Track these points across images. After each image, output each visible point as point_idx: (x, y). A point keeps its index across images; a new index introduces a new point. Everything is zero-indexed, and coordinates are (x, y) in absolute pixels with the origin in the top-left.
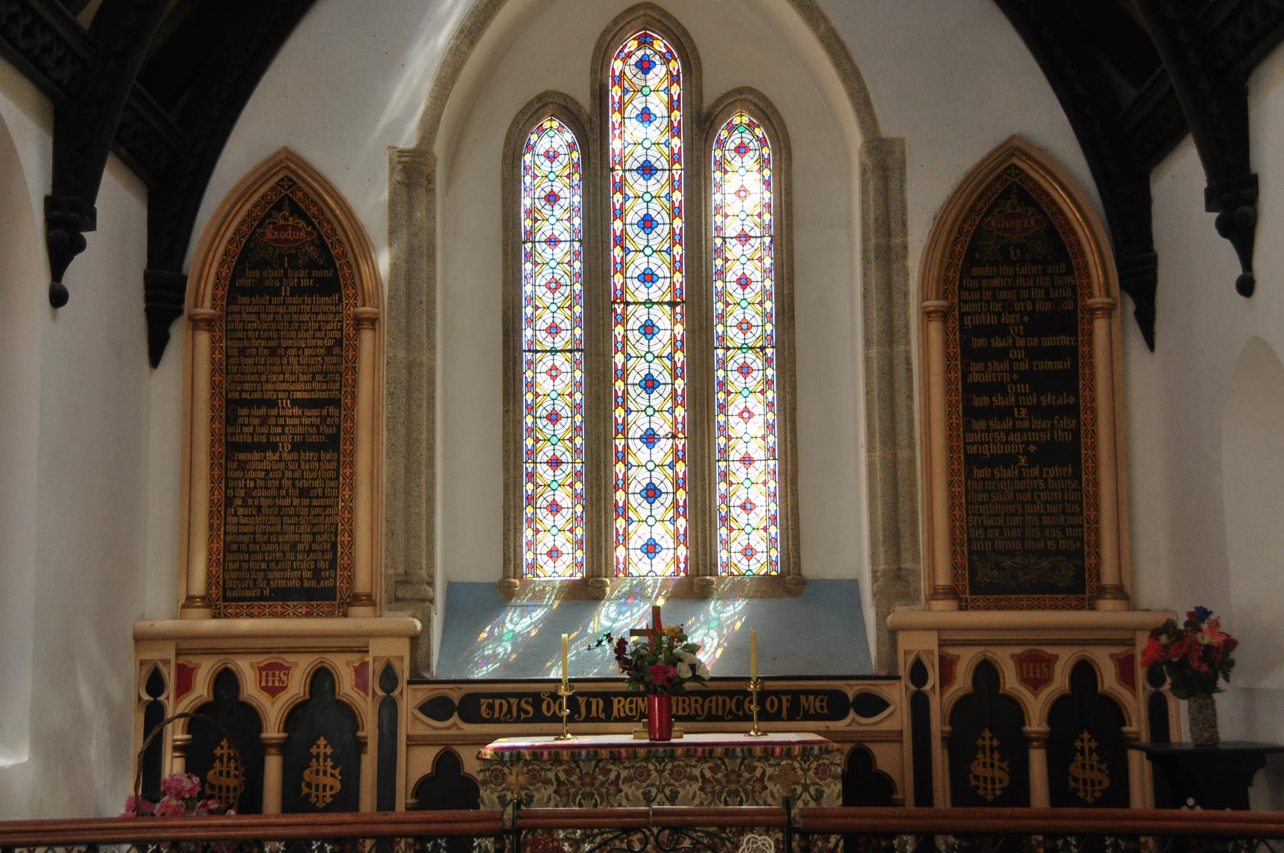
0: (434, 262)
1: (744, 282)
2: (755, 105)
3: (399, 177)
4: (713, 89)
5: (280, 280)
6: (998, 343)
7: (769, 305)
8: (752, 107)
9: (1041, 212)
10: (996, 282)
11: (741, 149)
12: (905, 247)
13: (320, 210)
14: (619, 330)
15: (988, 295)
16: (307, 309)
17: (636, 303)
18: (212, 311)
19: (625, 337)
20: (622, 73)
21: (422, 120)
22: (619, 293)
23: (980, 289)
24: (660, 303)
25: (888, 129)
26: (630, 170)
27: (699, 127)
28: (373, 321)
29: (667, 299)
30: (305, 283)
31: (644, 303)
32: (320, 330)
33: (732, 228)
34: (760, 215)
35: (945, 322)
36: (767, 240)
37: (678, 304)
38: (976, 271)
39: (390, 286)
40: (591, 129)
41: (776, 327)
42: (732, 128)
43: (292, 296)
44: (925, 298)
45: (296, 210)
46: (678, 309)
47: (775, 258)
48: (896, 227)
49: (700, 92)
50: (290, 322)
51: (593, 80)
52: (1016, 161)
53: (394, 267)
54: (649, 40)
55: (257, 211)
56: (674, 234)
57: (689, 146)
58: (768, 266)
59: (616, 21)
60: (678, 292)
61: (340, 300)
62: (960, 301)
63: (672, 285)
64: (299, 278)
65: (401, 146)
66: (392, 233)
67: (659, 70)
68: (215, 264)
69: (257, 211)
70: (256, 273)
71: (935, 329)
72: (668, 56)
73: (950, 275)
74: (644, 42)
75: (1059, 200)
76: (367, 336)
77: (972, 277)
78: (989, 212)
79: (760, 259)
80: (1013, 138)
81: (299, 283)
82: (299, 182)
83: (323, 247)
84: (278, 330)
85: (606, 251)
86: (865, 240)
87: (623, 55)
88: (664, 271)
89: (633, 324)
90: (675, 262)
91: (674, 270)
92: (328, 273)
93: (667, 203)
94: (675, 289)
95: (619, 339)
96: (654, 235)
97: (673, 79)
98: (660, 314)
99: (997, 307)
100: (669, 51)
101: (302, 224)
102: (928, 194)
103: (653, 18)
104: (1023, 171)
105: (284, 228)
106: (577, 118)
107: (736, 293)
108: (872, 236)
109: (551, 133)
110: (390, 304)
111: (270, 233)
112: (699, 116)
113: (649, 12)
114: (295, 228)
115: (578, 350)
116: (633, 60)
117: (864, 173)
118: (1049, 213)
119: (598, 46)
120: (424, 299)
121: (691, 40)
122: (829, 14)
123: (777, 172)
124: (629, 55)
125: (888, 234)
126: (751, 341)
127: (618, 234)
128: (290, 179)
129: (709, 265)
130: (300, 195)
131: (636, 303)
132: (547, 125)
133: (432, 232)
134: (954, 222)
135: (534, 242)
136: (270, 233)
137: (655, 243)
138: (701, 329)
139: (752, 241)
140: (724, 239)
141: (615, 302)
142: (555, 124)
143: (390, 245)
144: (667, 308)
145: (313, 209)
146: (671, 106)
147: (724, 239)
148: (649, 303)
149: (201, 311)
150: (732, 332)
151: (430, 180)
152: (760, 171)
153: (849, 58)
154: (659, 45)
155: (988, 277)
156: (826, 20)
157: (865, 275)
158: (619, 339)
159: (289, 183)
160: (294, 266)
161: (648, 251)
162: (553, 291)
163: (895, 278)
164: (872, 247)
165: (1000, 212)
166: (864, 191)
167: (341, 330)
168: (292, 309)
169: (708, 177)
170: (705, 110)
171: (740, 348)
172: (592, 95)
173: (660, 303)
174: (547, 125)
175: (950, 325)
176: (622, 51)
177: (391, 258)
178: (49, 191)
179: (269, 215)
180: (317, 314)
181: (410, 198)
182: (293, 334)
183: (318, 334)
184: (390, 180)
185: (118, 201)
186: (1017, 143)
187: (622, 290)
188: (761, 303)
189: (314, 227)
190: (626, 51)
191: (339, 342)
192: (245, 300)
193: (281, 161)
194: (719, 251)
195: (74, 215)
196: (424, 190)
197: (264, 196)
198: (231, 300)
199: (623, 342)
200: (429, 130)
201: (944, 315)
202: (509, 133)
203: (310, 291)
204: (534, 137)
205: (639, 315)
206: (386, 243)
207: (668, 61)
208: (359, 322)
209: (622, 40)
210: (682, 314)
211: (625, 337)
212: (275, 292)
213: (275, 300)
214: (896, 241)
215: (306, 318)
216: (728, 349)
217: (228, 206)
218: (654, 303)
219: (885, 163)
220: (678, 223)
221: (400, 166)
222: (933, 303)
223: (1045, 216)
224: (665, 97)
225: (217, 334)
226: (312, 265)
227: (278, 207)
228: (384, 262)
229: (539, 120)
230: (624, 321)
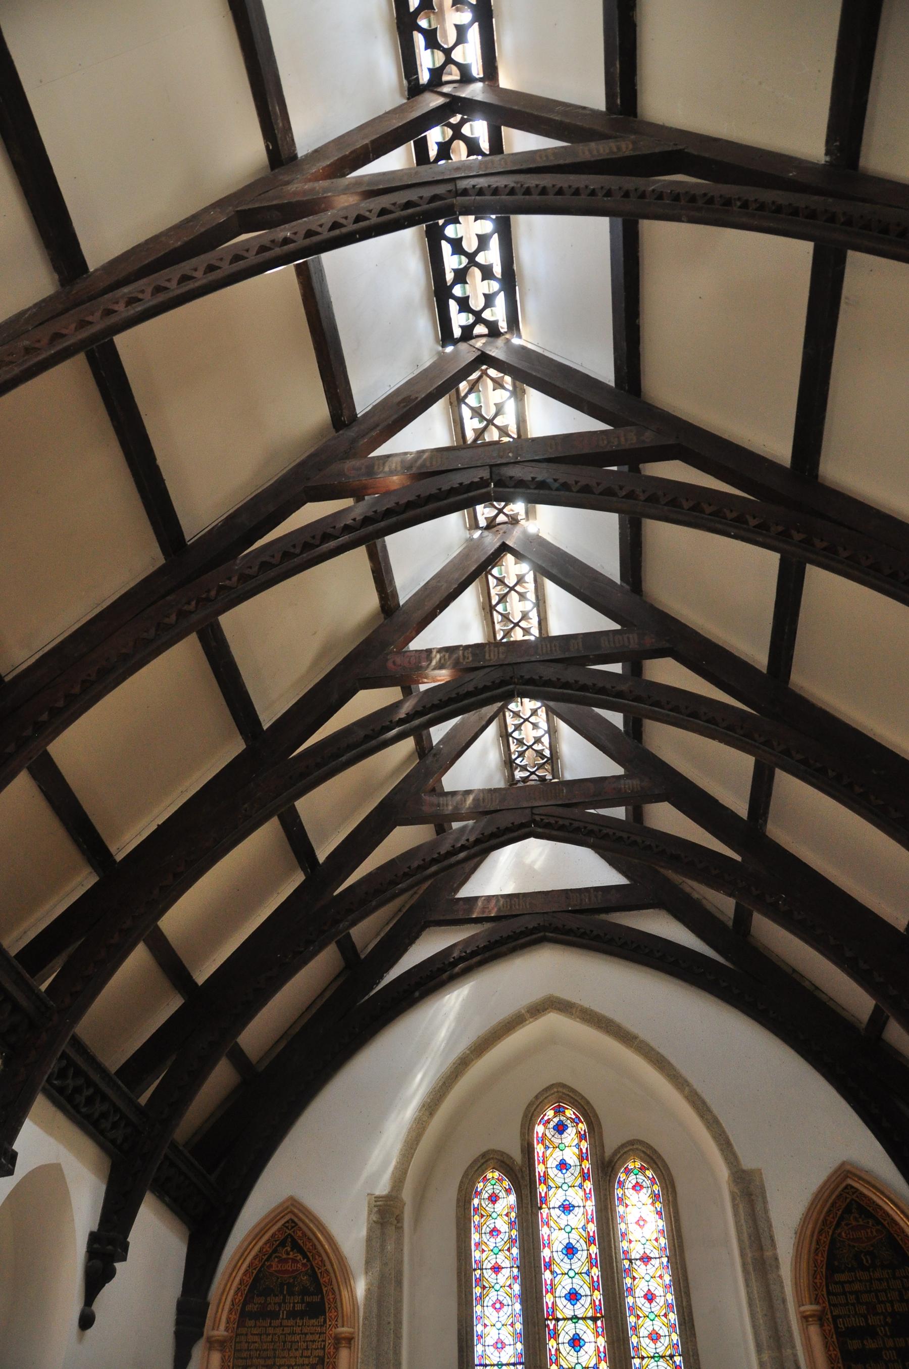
0: (401, 1288)
1: (650, 1297)
2: (643, 1152)
3: (374, 1217)
4: (611, 1143)
5: (280, 1305)
6: (870, 1344)
7: (673, 1317)
8: (642, 1155)
9: (878, 1222)
10: (857, 1287)
11: (637, 1187)
12: (777, 1259)
13: (314, 1246)
14: (552, 1344)
15: (852, 1299)
16: (298, 1330)
17: (564, 1319)
18: (226, 1333)
19: (558, 1350)
20: (544, 1135)
21: (393, 1173)
22: (550, 1311)
23: (844, 1293)
24: (584, 1319)
25: (748, 1162)
26: (554, 1208)
27: (604, 1173)
28: (350, 1340)
29: (590, 1315)
30: (298, 1307)
31: (571, 1319)
32: (307, 1349)
33: (636, 1251)
34: (656, 1240)
35: (822, 1326)
36: (665, 1260)
37: (598, 1318)
38: (839, 1277)
39: (364, 1308)
40: (523, 1177)
41: (680, 1336)
42: (628, 1172)
43: (288, 1318)
44: (800, 1303)
45: (296, 1246)
46: (599, 1323)
47: (672, 1276)
48: (766, 1242)
49: (602, 1146)
50: (285, 1342)
51: (522, 1140)
52: (849, 1181)
53: (368, 1291)
54: (562, 1109)
55: (267, 1248)
56: (591, 1258)
57: (597, 1187)
58: (667, 1282)
59: (537, 1097)
60: (598, 1308)
61: (325, 1322)
62: (830, 1304)
63: (593, 1302)
64: (294, 1303)
65: (378, 1192)
66: (368, 1263)
67: (571, 1132)
68: (232, 1292)
69: (267, 1248)
70: (262, 1300)
71: (814, 1331)
72: (577, 1120)
73: (818, 1281)
74: (559, 1111)
75: (891, 1212)
76: (344, 1354)
77: (836, 1283)
78: (838, 1225)
79: (661, 1277)
80: (843, 1163)
81: (294, 1307)
82: (301, 1224)
83: (314, 1276)
84: (274, 1350)
85: (538, 1275)
86: (743, 1255)
87: (543, 1121)
88: (585, 1290)
89: (564, 1338)
90: (593, 1282)
91: (594, 1289)
92: (316, 1299)
93: (584, 1233)
94: (595, 1305)
95: (553, 1352)
96: (575, 1260)
97: (582, 1137)
98: (585, 1328)
99: (863, 1309)
100: (577, 1117)
101: (299, 1257)
102: (788, 1211)
103: (564, 1093)
104: (857, 1190)
105: (285, 1261)
106: (511, 1169)
107: (645, 1306)
108: (748, 1251)
109: (493, 1182)
110: (364, 1324)
111: (275, 1265)
112: (603, 1163)
113: (560, 1089)
114: (294, 1261)
115: (520, 1363)
116: (552, 1125)
117: (733, 1199)
118: (885, 1223)
119: (525, 1115)
120: (391, 1319)
121: (593, 1108)
122: (691, 1080)
123: (666, 1204)
124: (548, 1121)
125: (761, 1248)
126: (661, 1350)
127: (547, 1260)
128: (293, 1221)
129: (621, 1283)
130: (299, 1233)
131: (564, 1319)
132: (489, 1175)
133: (400, 1262)
134: (812, 1236)
135: (482, 1269)
136: (275, 1265)
137: (576, 1267)
138: (618, 1340)
139: (653, 1261)
140: (630, 1260)
141: (547, 1319)
142: (496, 1174)
143: (366, 1273)
144: (590, 1322)
145: (309, 1245)
146: (581, 1158)
147: (630, 1260)
148: (575, 1318)
149: (215, 1333)
150: (645, 1342)
151: (399, 1219)
152: (653, 1204)
153: (709, 1110)
154: (569, 1113)
155: (850, 1282)
156: (688, 1085)
157: (747, 1285)
158: (553, 1352)
159: (292, 1224)
160: (291, 1293)
161: (572, 1274)
162: (498, 1310)
163: (772, 1287)
164: (749, 1260)
165: (847, 1225)
166: (736, 1214)
167: (324, 1349)
168: (287, 1330)
169: (613, 1211)
170: (607, 1159)
171: (653, 1357)
172: (522, 1151)
173: (584, 1319)
174: (489, 1175)
175: (826, 1328)
176: (543, 1118)
177: (367, 1284)
178: (95, 1228)
179: (275, 1251)
180: (306, 1334)
181: (383, 1234)
182: (285, 1353)
183: (306, 1353)
184: (368, 1220)
185: (155, 1235)
186: (848, 1167)
187: (553, 1308)
188: (665, 1315)
189: (309, 1260)
190: (546, 1118)
191: (321, 1360)
192: (251, 1323)
193: (287, 1207)
194: (628, 1271)
195: (110, 1247)
196: (394, 1228)
197: (273, 1236)
198: (241, 1323)
199: (556, 1355)
200: (398, 1181)
201: (820, 1319)
202: (461, 1182)
203: (302, 1314)
204: (480, 1186)
205: (567, 1330)
206: (363, 1272)
207: (577, 1124)
208: (338, 1341)
209: (543, 1112)
210: (602, 1327)
211: (558, 1350)
212: (274, 1315)
213: (276, 1323)
214: (768, 1254)
215: (297, 1338)
216: (643, 1358)
217: (246, 1244)
218: (579, 1319)
219: (748, 1190)
220: (594, 1249)
221: (376, 1209)
222: (809, 1308)
223: (883, 1226)
224: (577, 1151)
225: (227, 1355)
226: (305, 1292)
227: (283, 1244)
228: (360, 1288)
229: (484, 1172)
230: (555, 1335)
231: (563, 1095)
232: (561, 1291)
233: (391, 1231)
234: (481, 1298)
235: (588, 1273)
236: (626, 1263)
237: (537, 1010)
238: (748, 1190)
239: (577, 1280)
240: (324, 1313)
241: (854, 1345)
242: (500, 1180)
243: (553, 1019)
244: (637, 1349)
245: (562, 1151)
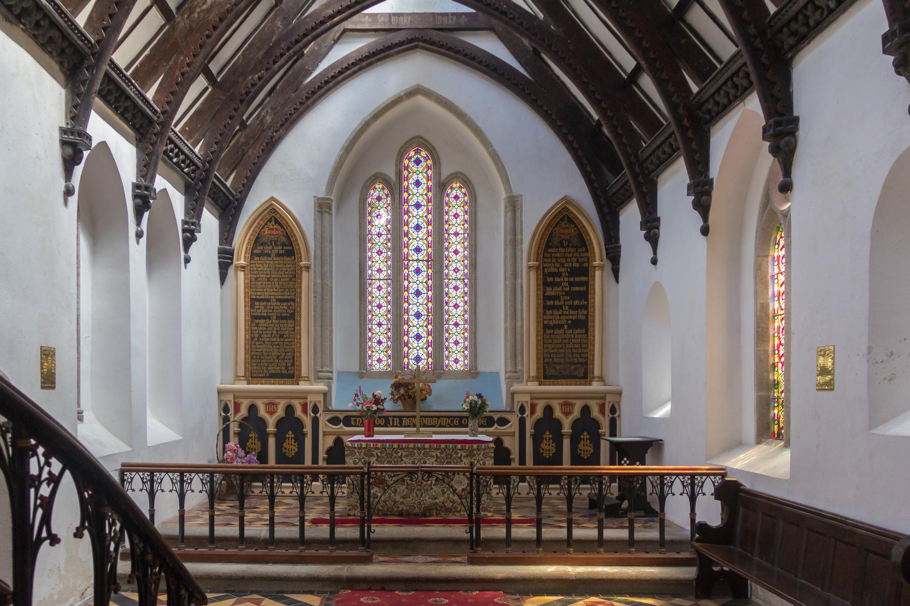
4: (446, 172)
6: (558, 280)
9: (576, 226)
10: (558, 255)
15: (554, 260)
27: (441, 187)
28: (308, 268)
30: (281, 252)
38: (550, 250)
44: (529, 260)
45: (277, 222)
48: (518, 232)
59: (406, 144)
70: (261, 248)
71: (533, 274)
74: (417, 152)
86: (505, 237)
92: (290, 248)
97: (429, 168)
99: (558, 265)
102: (533, 216)
105: (272, 229)
119: (398, 154)
124: (411, 158)
125: (515, 235)
126: (459, 276)
132: (377, 186)
136: (267, 231)
142: (381, 186)
154: (423, 154)
159: (274, 211)
160: (277, 245)
185: (209, 221)
201: (537, 268)
203: (283, 255)
204: (372, 191)
219: (514, 205)
222: (532, 263)
226: (283, 244)
231: (420, 142)
232: (412, 225)
233: (326, 216)
234: (370, 249)
235: (426, 173)
236: (446, 235)
237: (412, 93)
238: (514, 205)
239: (421, 243)
240: (294, 255)
241: (550, 279)
242: (383, 188)
243: (420, 99)
244: (447, 275)
245: (418, 179)
